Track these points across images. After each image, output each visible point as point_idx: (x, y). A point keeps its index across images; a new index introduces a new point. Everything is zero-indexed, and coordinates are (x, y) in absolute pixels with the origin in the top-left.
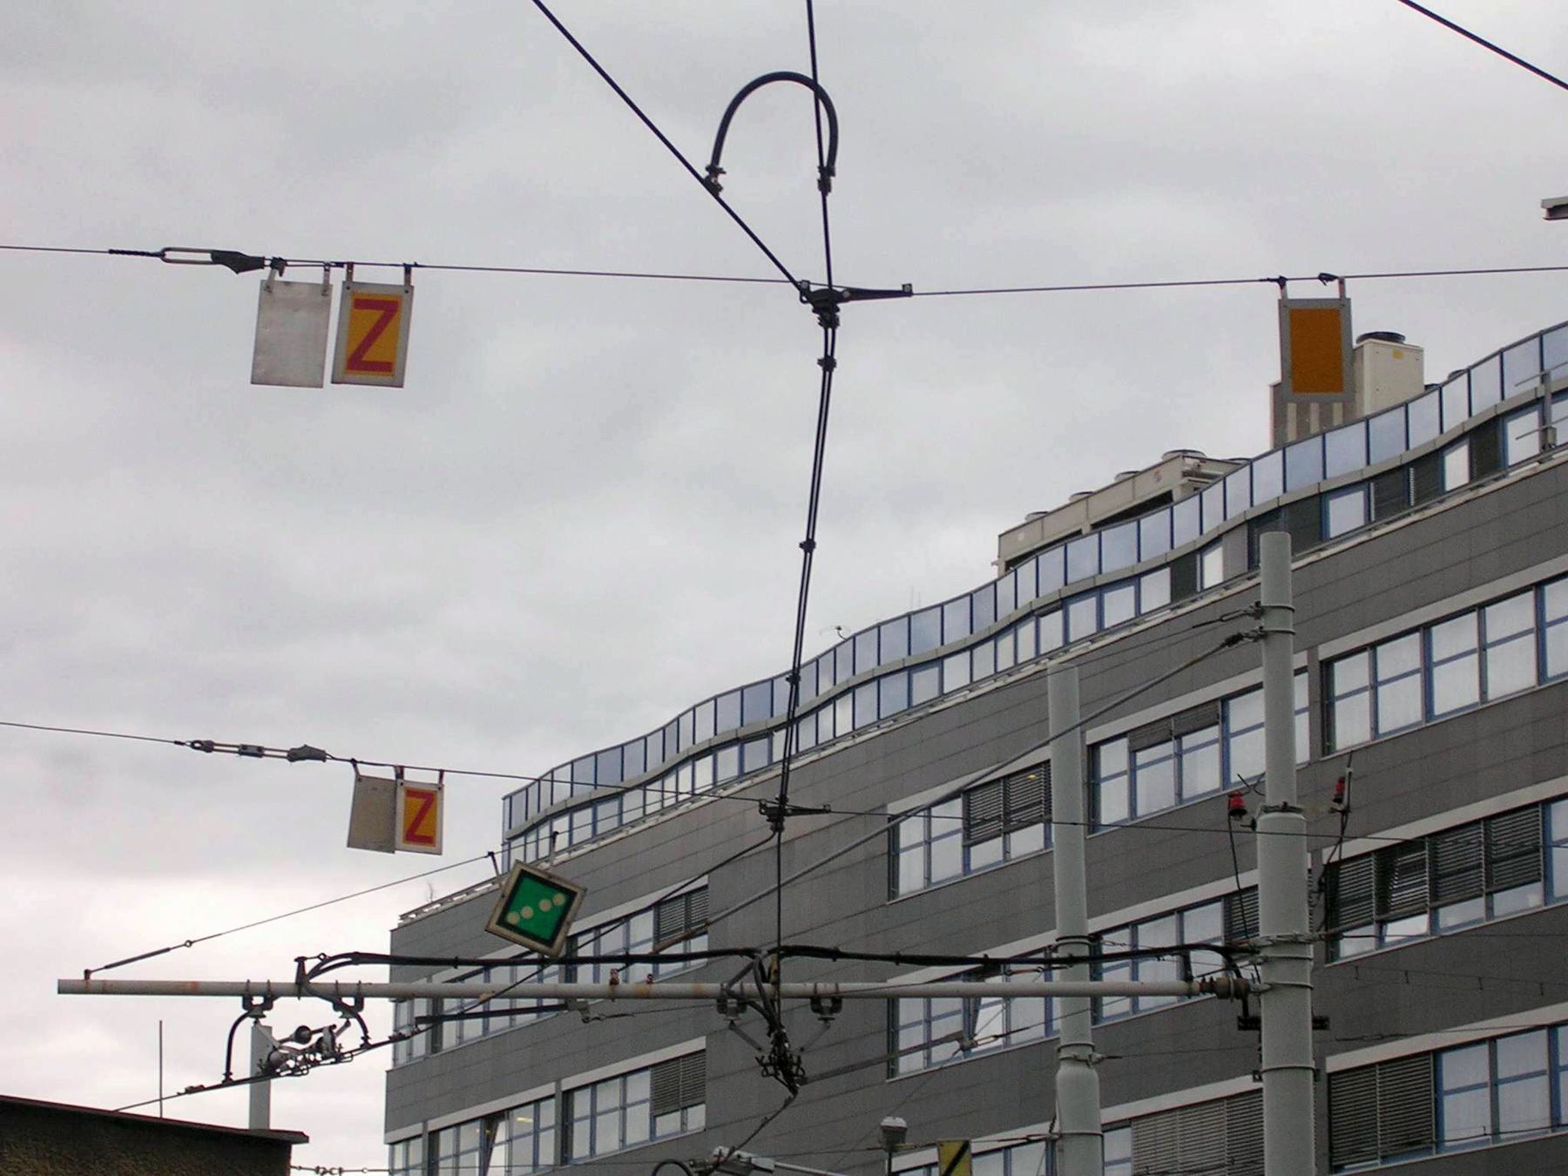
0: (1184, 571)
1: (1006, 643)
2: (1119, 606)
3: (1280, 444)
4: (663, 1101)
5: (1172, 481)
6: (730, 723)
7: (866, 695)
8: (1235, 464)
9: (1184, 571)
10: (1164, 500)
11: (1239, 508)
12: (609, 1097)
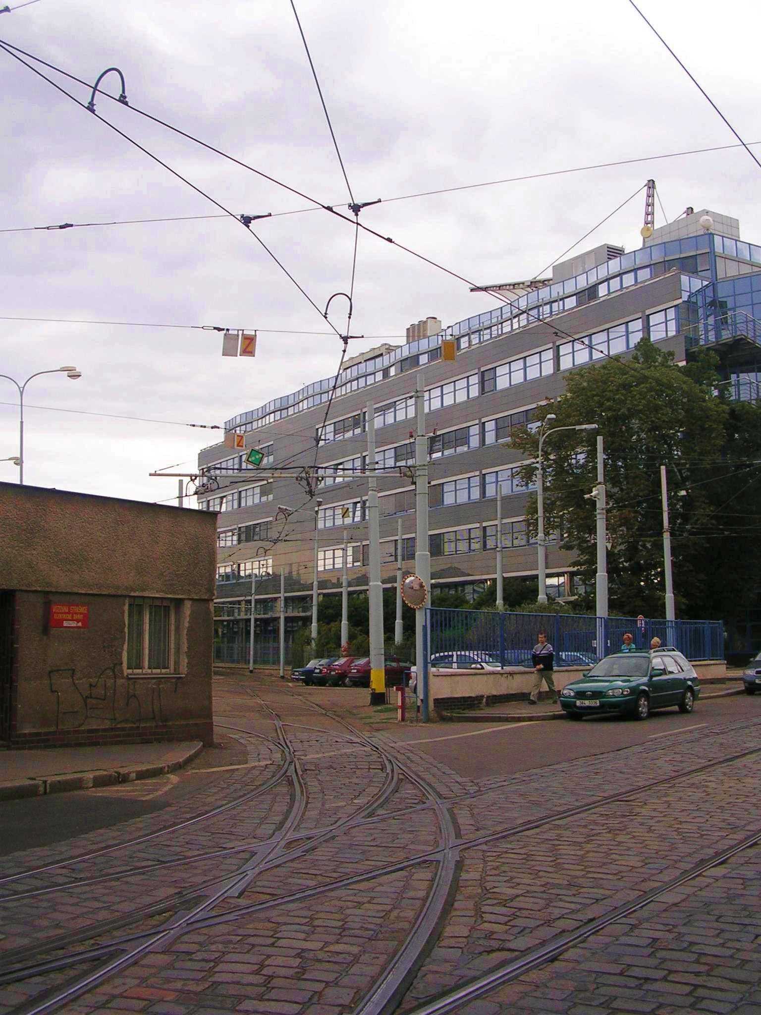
0: (386, 372)
1: (344, 388)
2: (370, 380)
3: (408, 343)
4: (262, 494)
5: (383, 351)
6: (278, 405)
7: (311, 399)
8: (398, 347)
9: (386, 372)
10: (382, 355)
11: (399, 357)
12: (250, 493)
